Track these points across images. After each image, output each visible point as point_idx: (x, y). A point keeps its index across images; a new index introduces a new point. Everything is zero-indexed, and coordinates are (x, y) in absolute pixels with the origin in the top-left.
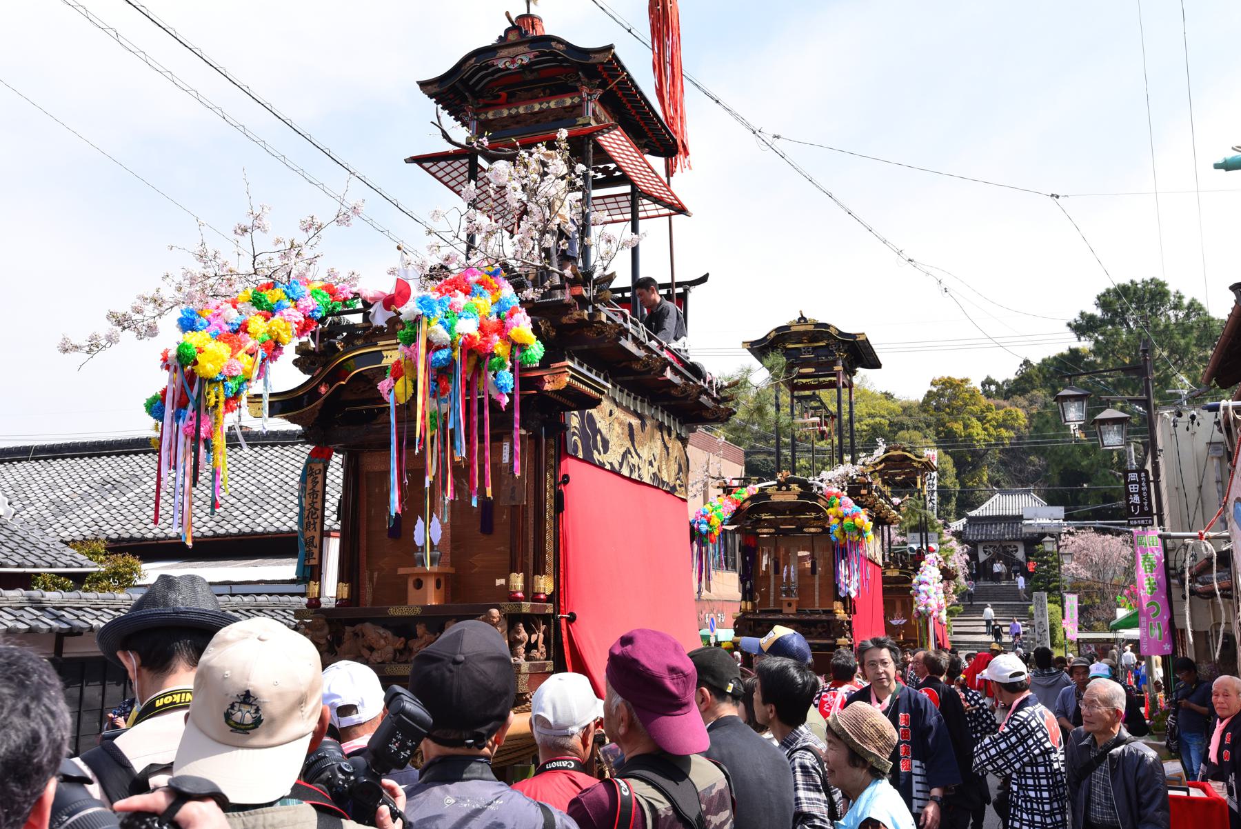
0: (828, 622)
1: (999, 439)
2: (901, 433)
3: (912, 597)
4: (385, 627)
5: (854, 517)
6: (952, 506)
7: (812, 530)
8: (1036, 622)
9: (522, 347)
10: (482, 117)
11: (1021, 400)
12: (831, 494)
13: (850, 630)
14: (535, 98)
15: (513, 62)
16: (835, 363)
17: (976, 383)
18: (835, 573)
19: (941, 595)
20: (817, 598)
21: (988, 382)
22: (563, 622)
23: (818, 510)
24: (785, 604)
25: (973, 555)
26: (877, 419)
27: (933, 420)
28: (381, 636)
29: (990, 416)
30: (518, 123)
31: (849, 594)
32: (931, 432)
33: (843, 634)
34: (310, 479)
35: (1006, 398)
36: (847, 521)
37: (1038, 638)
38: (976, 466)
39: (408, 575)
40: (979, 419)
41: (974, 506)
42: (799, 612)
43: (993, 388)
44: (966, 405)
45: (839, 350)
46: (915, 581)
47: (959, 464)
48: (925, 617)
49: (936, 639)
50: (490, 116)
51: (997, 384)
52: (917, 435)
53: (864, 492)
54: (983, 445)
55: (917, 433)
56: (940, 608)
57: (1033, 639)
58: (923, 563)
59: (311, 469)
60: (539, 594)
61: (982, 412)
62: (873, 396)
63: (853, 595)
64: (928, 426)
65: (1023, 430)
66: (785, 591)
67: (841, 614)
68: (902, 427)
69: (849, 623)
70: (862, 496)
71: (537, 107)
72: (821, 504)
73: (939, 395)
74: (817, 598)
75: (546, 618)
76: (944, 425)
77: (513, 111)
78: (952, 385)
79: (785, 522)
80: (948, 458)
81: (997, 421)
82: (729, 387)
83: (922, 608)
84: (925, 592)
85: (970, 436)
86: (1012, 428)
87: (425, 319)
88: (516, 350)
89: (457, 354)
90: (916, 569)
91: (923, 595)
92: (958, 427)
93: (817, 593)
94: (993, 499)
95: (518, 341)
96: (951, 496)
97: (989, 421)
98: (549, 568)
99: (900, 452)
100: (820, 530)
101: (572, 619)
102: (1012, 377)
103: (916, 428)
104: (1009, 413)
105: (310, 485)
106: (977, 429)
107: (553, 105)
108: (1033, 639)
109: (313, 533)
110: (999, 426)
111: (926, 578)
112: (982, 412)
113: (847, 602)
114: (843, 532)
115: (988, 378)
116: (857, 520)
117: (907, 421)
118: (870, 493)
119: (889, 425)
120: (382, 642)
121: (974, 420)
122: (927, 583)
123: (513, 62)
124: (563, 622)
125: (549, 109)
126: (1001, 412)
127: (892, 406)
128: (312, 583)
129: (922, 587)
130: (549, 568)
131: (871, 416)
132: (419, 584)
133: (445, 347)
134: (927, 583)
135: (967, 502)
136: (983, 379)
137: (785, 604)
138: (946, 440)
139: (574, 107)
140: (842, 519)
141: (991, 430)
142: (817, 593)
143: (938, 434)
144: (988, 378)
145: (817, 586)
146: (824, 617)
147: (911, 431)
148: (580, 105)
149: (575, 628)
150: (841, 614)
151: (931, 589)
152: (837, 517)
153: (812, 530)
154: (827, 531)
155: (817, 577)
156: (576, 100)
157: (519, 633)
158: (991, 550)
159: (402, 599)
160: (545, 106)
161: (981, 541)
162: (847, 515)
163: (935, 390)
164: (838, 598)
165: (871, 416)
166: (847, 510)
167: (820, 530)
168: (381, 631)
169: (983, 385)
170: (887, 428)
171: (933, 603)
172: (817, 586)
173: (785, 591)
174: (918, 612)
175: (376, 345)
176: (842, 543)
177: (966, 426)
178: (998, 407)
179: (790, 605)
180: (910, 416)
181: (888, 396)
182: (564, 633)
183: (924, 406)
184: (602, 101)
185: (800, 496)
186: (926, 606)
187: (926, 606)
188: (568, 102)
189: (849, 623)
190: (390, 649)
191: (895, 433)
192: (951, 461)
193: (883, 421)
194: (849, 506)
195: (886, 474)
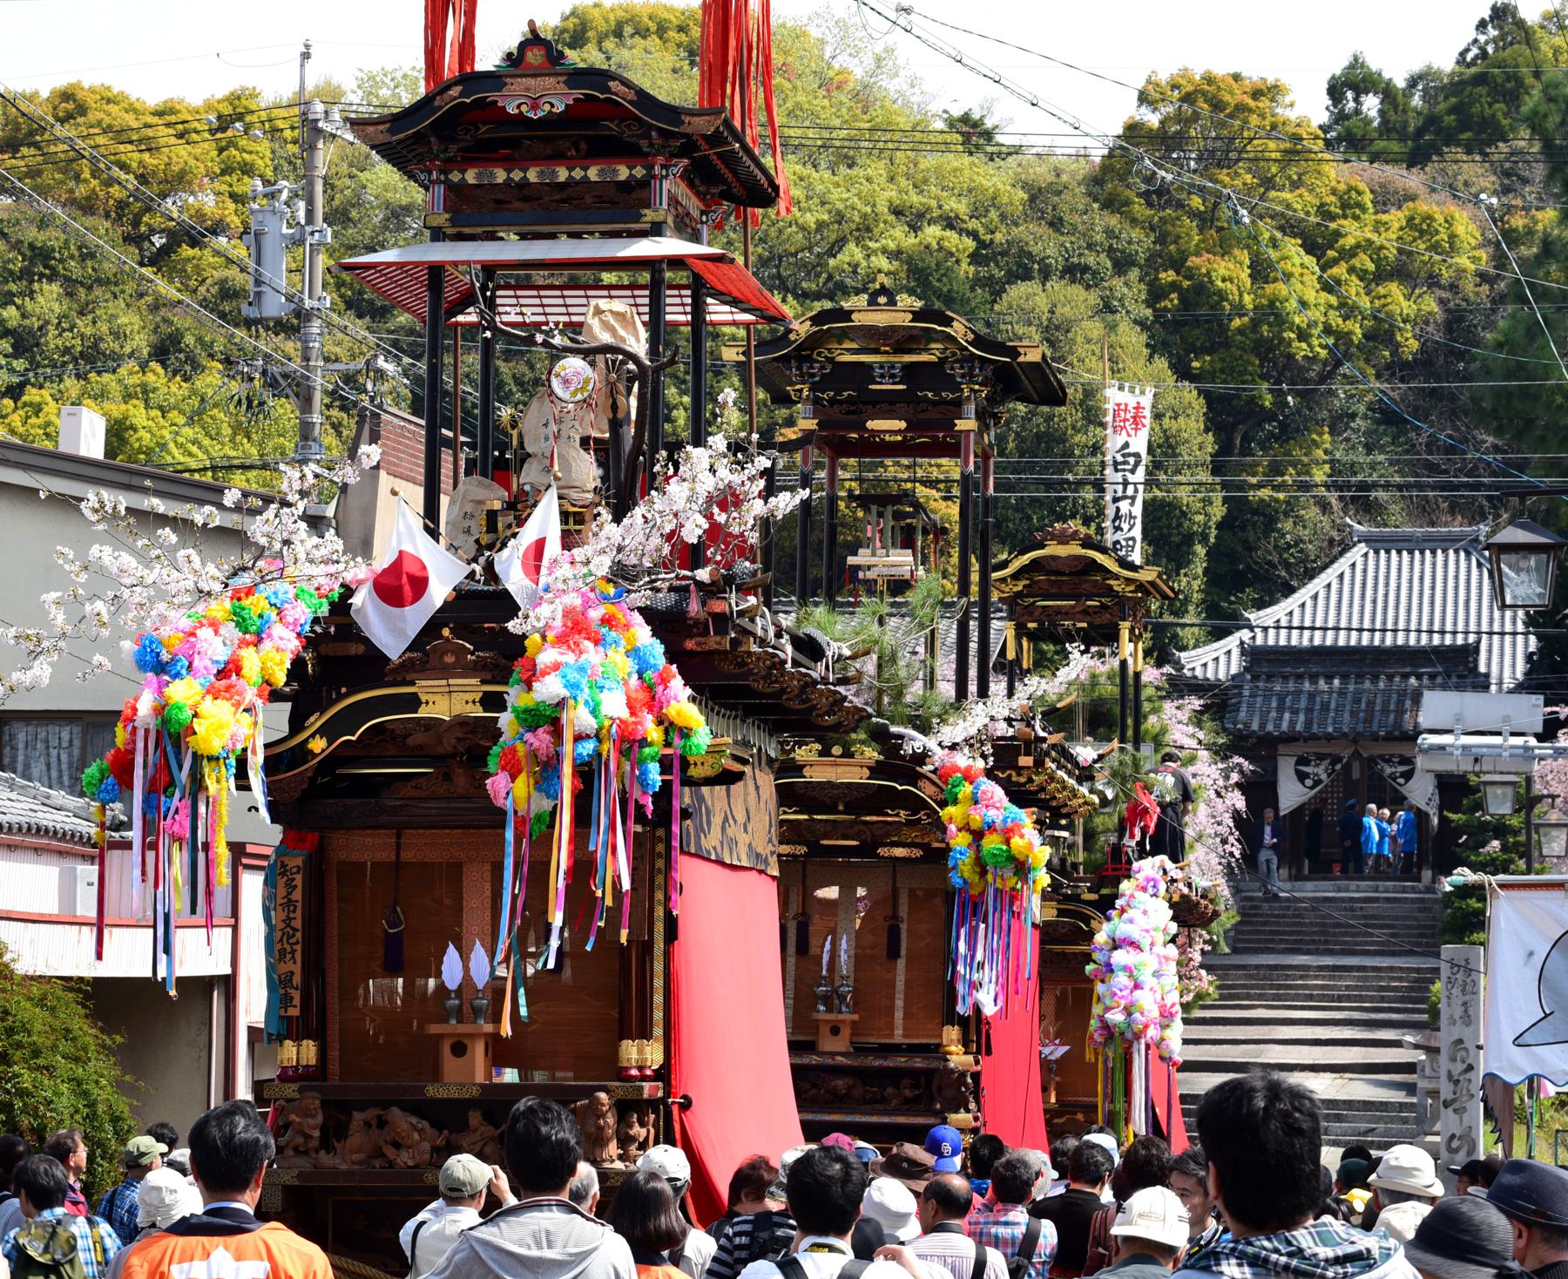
0: (929, 1074)
1: (1381, 332)
2: (1017, 292)
3: (1090, 981)
4: (422, 1116)
5: (1008, 834)
6: (1192, 581)
7: (899, 852)
8: (1444, 1038)
9: (685, 733)
10: (455, 177)
11: (1474, 172)
12: (956, 769)
13: (977, 1093)
14: (559, 157)
15: (535, 107)
16: (957, 407)
17: (1309, 107)
18: (950, 958)
19: (1171, 980)
20: (899, 1015)
21: (1351, 82)
22: (675, 1110)
23: (915, 804)
24: (825, 1030)
25: (1259, 790)
26: (932, 233)
27: (1139, 241)
28: (414, 1128)
29: (1353, 232)
30: (525, 199)
31: (977, 1009)
32: (1130, 290)
33: (959, 1104)
34: (281, 882)
35: (1415, 159)
36: (991, 843)
37: (1446, 1091)
38: (1290, 430)
39: (440, 1036)
40: (1311, 248)
41: (1275, 589)
42: (859, 1050)
43: (1371, 104)
44: (1268, 183)
45: (970, 376)
46: (1101, 938)
47: (1230, 420)
48: (1122, 1041)
49: (1150, 1107)
50: (471, 177)
51: (1388, 93)
52: (1074, 300)
53: (1025, 761)
54: (1319, 346)
55: (1077, 291)
56: (1166, 1015)
57: (1434, 1094)
58: (1125, 886)
59: (283, 865)
60: (627, 1069)
61: (1324, 212)
62: (917, 138)
63: (989, 1010)
64: (1122, 264)
65: (1469, 286)
66: (826, 1000)
67: (959, 1058)
68: (1024, 267)
69: (976, 1076)
70: (1019, 770)
71: (562, 174)
72: (926, 792)
73: (1165, 141)
74: (899, 1015)
75: (653, 1104)
76: (1178, 264)
77: (517, 175)
78: (1217, 105)
79: (834, 829)
80: (1189, 394)
81: (1375, 251)
82: (854, 657)
83: (1116, 1017)
84: (1127, 969)
85: (1272, 312)
86: (1433, 281)
87: (571, 702)
88: (674, 736)
89: (607, 747)
90: (1106, 905)
91: (1121, 979)
92: (1229, 273)
93: (899, 1003)
94: (1342, 565)
95: (679, 722)
96: (1189, 539)
97: (1348, 254)
98: (658, 1031)
99: (1075, 549)
100: (917, 853)
101: (686, 1105)
102: (1446, 63)
103: (1074, 272)
104: (1420, 227)
105: (282, 892)
106: (1302, 287)
107: (593, 174)
108: (1434, 1094)
109: (290, 966)
110: (1381, 276)
111: (1133, 932)
112: (1324, 212)
113: (976, 1030)
114: (981, 866)
115: (1356, 63)
116: (1016, 841)
117: (1047, 245)
118: (1039, 763)
119: (975, 258)
120: (416, 1136)
121: (1293, 248)
122: (1134, 944)
123: (535, 107)
124: (675, 1110)
125: (585, 181)
126: (1396, 218)
127: (996, 179)
128: (288, 1043)
129: (1120, 957)
130: (658, 1031)
131: (915, 220)
132: (460, 1049)
133: (588, 736)
134: (1134, 944)
135: (1250, 564)
136: (1337, 67)
137: (825, 1030)
138: (1189, 331)
139: (627, 186)
140: (978, 835)
141: (1353, 288)
142: (899, 1003)
143: (1156, 294)
144: (1356, 63)
145: (900, 984)
146: (918, 1063)
147: (1055, 285)
148: (645, 184)
149: (689, 1117)
150: (959, 1058)
151: (1145, 963)
152: (966, 828)
153: (899, 852)
154: (938, 856)
155: (901, 963)
156: (639, 172)
157: (631, 1127)
158: (1320, 771)
159: (436, 1075)
160: (578, 174)
161: (1290, 738)
162: (991, 827)
163: (1153, 119)
164: (951, 1018)
165: (915, 220)
166: (992, 814)
167: (917, 853)
168: (414, 1120)
169: (1335, 90)
170: (966, 269)
171: (1148, 1002)
172: (900, 984)
173: (826, 1000)
174: (1106, 1027)
175: (413, 683)
176: (975, 892)
177: (1261, 271)
178: (1386, 199)
179: (835, 1031)
180: (1056, 224)
181: (972, 133)
182: (677, 1127)
183: (1110, 179)
184: (688, 178)
185: (876, 770)
186: (1128, 1011)
187: (1128, 1011)
188: (623, 173)
189: (976, 1076)
190: (426, 1146)
191: (997, 291)
192: (1199, 405)
193: (953, 239)
194: (997, 805)
195: (1030, 611)
